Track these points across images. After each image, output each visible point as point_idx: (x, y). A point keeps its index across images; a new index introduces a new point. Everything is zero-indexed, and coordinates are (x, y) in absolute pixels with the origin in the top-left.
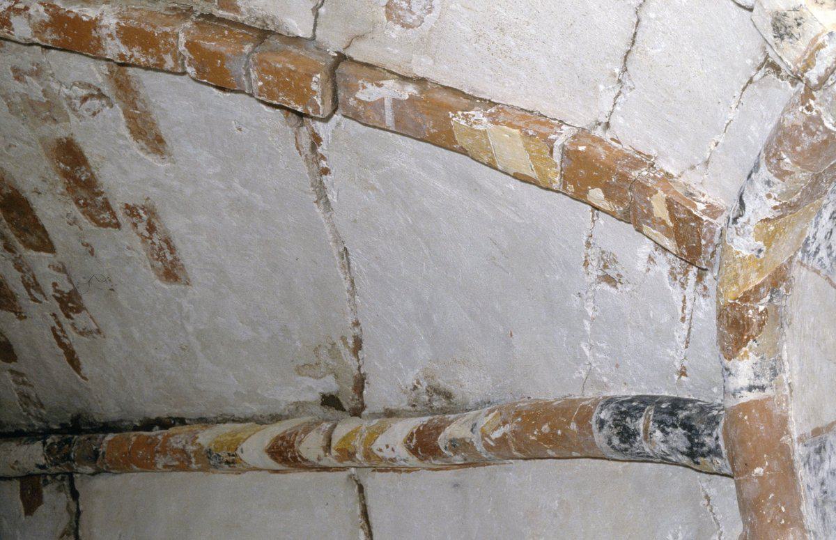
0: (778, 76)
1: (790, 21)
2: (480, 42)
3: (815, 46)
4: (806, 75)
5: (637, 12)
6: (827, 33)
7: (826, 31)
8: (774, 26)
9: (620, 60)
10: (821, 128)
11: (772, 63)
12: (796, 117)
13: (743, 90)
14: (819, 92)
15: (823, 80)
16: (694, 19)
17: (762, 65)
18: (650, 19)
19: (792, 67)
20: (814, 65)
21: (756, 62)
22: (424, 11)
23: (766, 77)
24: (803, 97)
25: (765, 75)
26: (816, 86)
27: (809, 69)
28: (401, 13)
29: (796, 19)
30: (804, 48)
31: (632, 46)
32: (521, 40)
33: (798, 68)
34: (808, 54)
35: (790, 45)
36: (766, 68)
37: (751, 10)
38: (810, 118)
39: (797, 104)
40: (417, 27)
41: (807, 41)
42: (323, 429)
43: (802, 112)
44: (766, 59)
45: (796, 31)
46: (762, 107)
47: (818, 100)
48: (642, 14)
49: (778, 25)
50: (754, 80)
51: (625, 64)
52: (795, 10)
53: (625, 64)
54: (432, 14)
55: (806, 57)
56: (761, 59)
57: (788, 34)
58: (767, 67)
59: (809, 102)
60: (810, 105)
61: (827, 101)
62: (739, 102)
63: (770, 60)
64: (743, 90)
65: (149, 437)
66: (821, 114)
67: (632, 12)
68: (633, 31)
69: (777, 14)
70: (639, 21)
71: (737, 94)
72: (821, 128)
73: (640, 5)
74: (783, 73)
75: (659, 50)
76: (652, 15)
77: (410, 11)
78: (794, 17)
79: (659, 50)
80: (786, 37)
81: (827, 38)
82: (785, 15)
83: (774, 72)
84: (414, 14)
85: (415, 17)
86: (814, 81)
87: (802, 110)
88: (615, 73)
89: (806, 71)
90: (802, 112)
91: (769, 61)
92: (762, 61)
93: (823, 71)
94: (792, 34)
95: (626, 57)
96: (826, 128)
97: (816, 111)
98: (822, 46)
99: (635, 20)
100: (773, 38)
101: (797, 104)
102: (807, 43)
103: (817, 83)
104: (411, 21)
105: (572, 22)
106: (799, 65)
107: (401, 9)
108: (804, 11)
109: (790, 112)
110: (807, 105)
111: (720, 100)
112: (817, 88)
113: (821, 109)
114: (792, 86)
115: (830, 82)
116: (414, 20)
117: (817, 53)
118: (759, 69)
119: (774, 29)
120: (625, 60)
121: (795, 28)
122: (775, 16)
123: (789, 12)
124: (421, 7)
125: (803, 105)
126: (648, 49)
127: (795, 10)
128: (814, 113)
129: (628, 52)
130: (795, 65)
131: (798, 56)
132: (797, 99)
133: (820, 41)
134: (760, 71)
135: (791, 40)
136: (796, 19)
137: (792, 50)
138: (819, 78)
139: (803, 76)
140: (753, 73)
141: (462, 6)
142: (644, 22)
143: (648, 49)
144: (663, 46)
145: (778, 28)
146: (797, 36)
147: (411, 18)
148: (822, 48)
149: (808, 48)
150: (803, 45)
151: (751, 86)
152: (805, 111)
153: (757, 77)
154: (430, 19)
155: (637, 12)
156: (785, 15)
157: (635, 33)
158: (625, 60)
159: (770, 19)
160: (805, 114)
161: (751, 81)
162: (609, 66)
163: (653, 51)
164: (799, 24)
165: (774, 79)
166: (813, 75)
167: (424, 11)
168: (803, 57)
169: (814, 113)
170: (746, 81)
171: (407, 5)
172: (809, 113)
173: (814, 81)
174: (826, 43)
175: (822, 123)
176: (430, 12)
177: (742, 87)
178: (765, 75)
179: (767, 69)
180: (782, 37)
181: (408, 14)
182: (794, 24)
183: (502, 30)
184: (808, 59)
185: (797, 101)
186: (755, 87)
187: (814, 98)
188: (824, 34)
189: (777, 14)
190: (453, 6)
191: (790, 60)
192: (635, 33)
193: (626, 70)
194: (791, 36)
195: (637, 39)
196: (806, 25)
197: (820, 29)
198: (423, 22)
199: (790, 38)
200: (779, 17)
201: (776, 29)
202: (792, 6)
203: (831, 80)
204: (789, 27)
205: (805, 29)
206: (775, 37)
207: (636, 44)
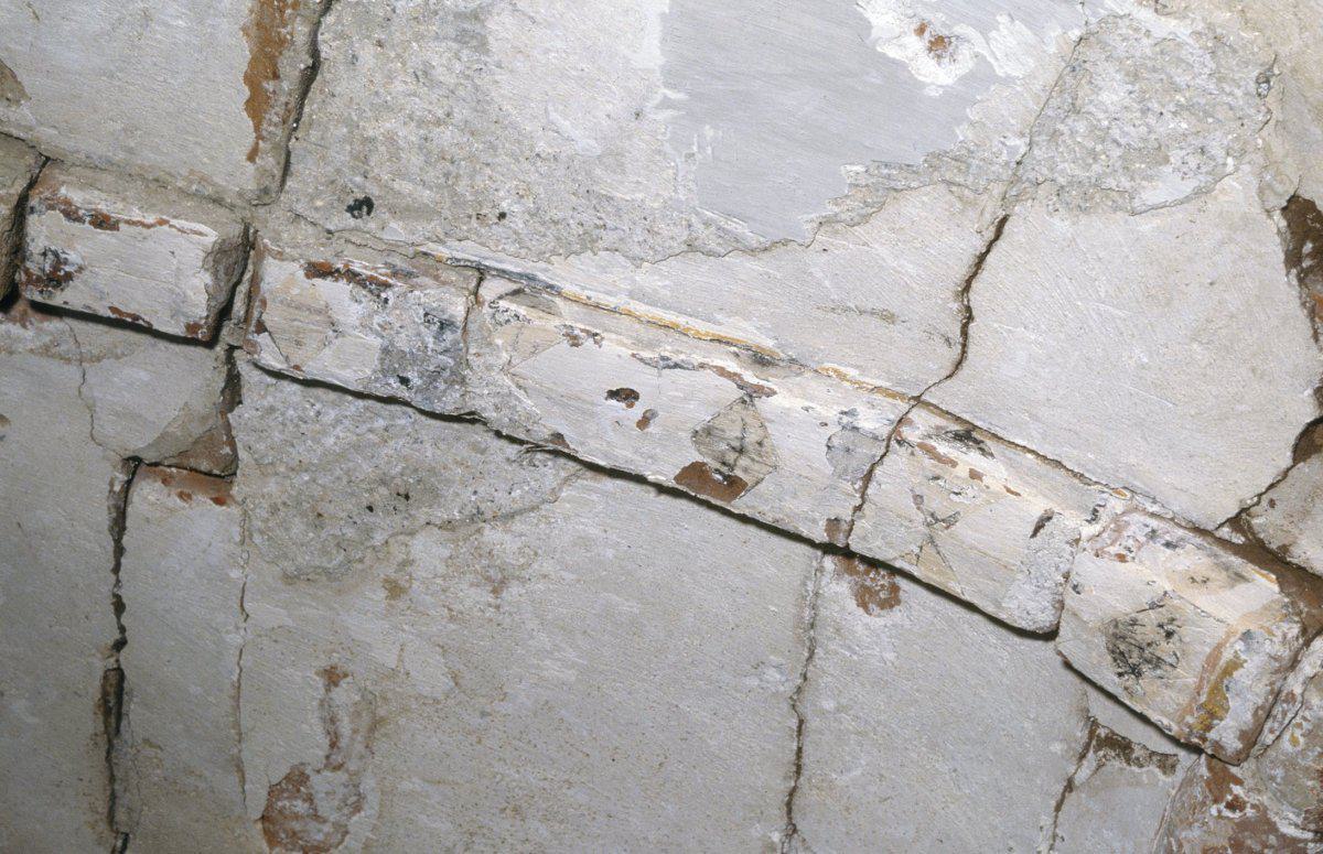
0: (1128, 761)
1: (1148, 631)
2: (476, 847)
3: (1218, 670)
4: (1212, 735)
5: (794, 706)
6: (1238, 636)
7: (1234, 633)
8: (1113, 652)
9: (777, 812)
10: (1272, 839)
11: (1106, 737)
12: (1208, 832)
13: (1058, 808)
14: (1245, 764)
15: (1250, 738)
16: (918, 691)
17: (1087, 747)
18: (823, 713)
19: (1175, 728)
20: (1227, 711)
21: (1073, 745)
22: (346, 811)
23: (1103, 768)
24: (1212, 786)
25: (1100, 766)
26: (1239, 752)
27: (1215, 722)
28: (297, 826)
29: (1161, 626)
30: (1192, 680)
31: (798, 778)
32: (561, 822)
33: (1190, 727)
34: (1206, 689)
35: (1159, 682)
36: (1095, 752)
37: (1050, 635)
38: (1244, 825)
39: (1204, 804)
40: (336, 847)
41: (1197, 663)
42: (367, 184)
43: (1220, 816)
44: (1092, 733)
45: (1165, 649)
46: (1107, 834)
47: (1249, 783)
48: (807, 709)
49: (1122, 647)
50: (1077, 782)
51: (790, 819)
52: (1153, 606)
53: (790, 819)
54: (363, 813)
55: (1203, 698)
56: (1081, 734)
57: (1149, 662)
58: (1099, 747)
59: (1231, 792)
60: (1236, 798)
61: (1272, 778)
62: (1055, 836)
63: (1102, 732)
64: (1058, 808)
65: (688, 485)
66: (1266, 809)
67: (785, 707)
68: (794, 746)
69: (1116, 626)
70: (801, 722)
71: (1046, 821)
72: (1272, 839)
73: (799, 690)
74: (1138, 752)
75: (858, 772)
76: (829, 705)
77: (316, 817)
78: (1156, 623)
79: (858, 772)
80: (1145, 668)
81: (1240, 646)
82: (1134, 622)
83: (1118, 755)
84: (325, 821)
85: (327, 828)
86: (1232, 743)
87: (1219, 812)
88: (773, 843)
89: (1209, 728)
90: (1220, 816)
91: (1098, 736)
92: (1085, 739)
93: (1249, 716)
94: (1159, 658)
95: (789, 805)
96: (1284, 836)
97: (1253, 806)
98: (1235, 664)
99: (794, 723)
100: (1116, 679)
101: (1204, 804)
102: (1199, 669)
103: (1241, 746)
104: (320, 837)
105: (661, 759)
106: (1190, 719)
107: (297, 817)
108: (1176, 602)
109: (1190, 825)
110: (1229, 798)
111: (1012, 843)
112: (1241, 757)
113: (1265, 799)
114: (1165, 773)
115: (1268, 738)
116: (327, 834)
117: (1226, 682)
118: (1082, 757)
119: (1115, 660)
120: (789, 811)
121: (1164, 644)
122: (1111, 630)
123: (1140, 616)
124: (336, 803)
125: (1216, 801)
126: (834, 776)
127: (1153, 606)
128: (1249, 812)
129: (792, 793)
130: (1181, 721)
131: (1184, 700)
132: (1198, 791)
133: (1227, 655)
134: (1085, 762)
135: (1159, 672)
136: (1161, 626)
137: (1168, 692)
138: (1243, 735)
139: (1204, 740)
140: (1072, 769)
141: (424, 780)
142: (813, 723)
143: (834, 776)
144: (863, 763)
145: (1122, 653)
146: (1172, 660)
147: (319, 831)
148: (1236, 669)
149: (1202, 679)
150: (1187, 676)
151: (1072, 798)
152: (1227, 813)
153: (1083, 774)
154: (359, 824)
155: (794, 706)
156: (1134, 622)
157: (800, 750)
158: (789, 811)
159: (1101, 642)
160: (1228, 818)
161: (1070, 786)
162: (756, 831)
163: (844, 778)
164: (1169, 635)
165: (1121, 769)
166: (1227, 733)
167: (346, 811)
168: (1194, 699)
169: (1249, 812)
170: (1060, 788)
171: (306, 805)
172: (1237, 815)
173: (1232, 743)
174: (1243, 657)
175: (1273, 828)
176: (357, 808)
177: (1053, 803)
178: (1100, 766)
179: (1101, 753)
180: (1136, 672)
181: (313, 825)
182: (1159, 636)
183: (516, 810)
184: (1209, 700)
185: (1200, 798)
186: (1083, 795)
187: (1239, 782)
188: (1232, 640)
189: (1116, 626)
190: (406, 786)
191: (1163, 713)
192: (800, 750)
193: (795, 831)
194: (1157, 662)
195: (805, 760)
196: (1187, 632)
197: (1221, 632)
198: (347, 832)
199: (1157, 667)
200: (1122, 629)
201: (1119, 656)
202: (1145, 600)
203: (1271, 731)
204: (1149, 645)
205: (1187, 639)
206: (1120, 675)
207: (806, 773)
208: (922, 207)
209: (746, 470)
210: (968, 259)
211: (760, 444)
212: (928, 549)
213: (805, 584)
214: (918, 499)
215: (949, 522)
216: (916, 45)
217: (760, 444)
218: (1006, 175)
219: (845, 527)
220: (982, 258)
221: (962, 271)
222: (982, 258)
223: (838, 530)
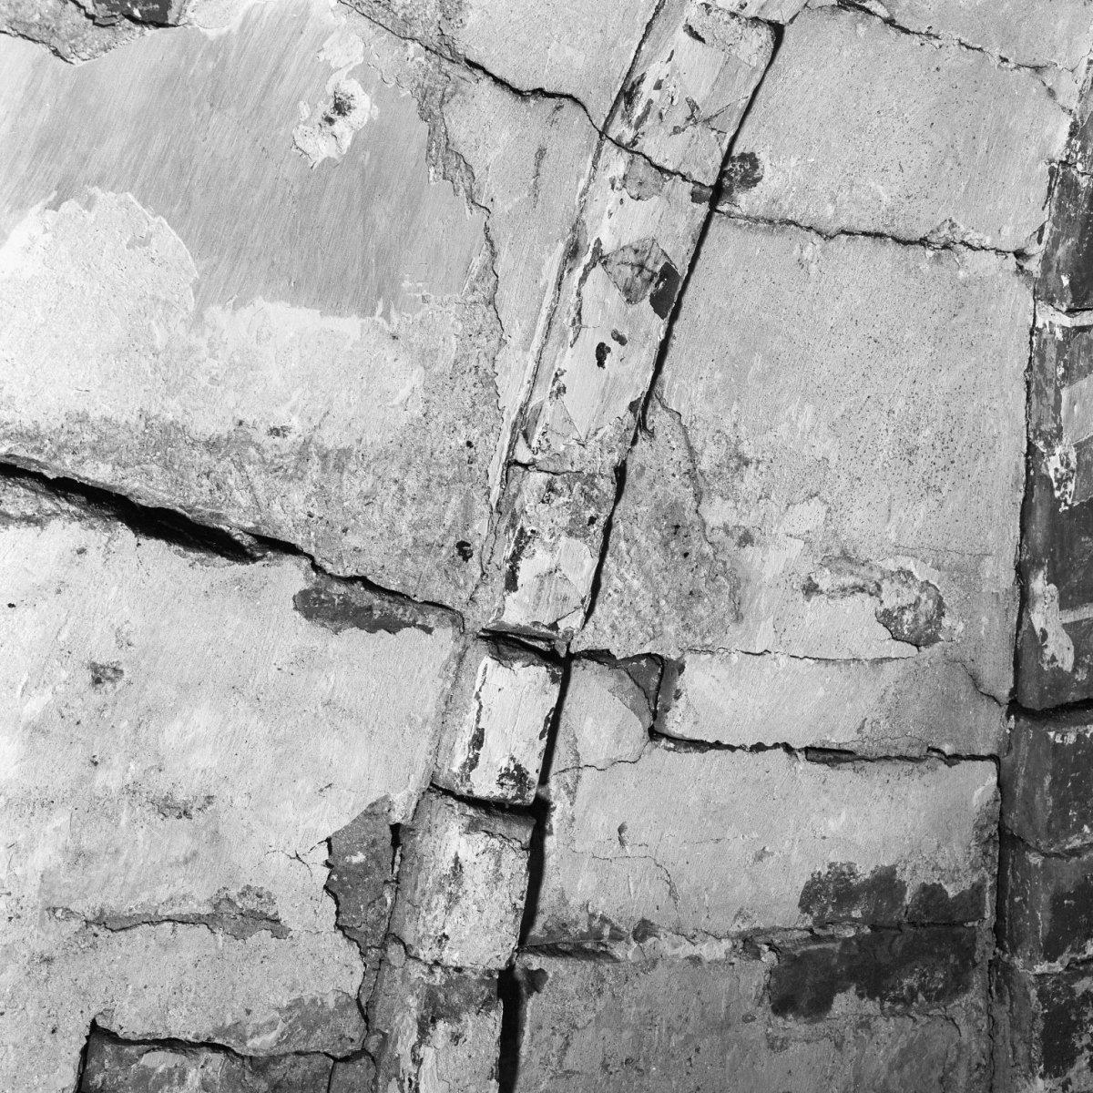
13: (907, 31)
64: (907, 31)
67: (832, 243)
70: (843, 232)
157: (864, 234)
192: (864, 234)
208: (460, 125)
209: (656, 263)
210: (497, 90)
211: (636, 251)
212: (713, 124)
213: (740, 226)
214: (676, 130)
215: (693, 106)
216: (341, 125)
217: (636, 251)
218: (435, 59)
219: (698, 188)
220: (498, 81)
221: (507, 97)
222: (498, 81)
223: (700, 193)
